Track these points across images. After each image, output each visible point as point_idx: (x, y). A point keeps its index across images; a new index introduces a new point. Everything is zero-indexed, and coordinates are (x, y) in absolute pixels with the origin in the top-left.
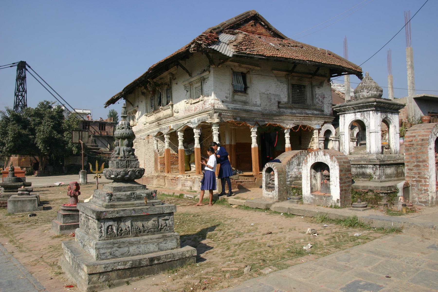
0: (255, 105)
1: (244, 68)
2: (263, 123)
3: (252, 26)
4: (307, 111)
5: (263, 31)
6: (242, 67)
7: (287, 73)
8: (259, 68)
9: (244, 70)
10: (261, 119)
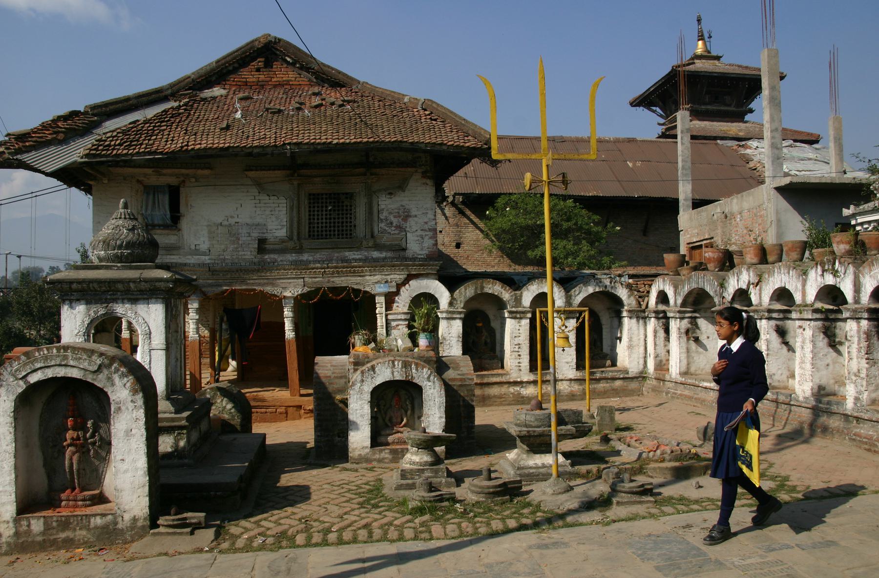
0: (197, 252)
1: (171, 175)
2: (218, 290)
3: (258, 70)
4: (347, 254)
5: (291, 75)
6: (165, 175)
7: (288, 172)
8: (206, 172)
9: (173, 181)
10: (210, 281)
